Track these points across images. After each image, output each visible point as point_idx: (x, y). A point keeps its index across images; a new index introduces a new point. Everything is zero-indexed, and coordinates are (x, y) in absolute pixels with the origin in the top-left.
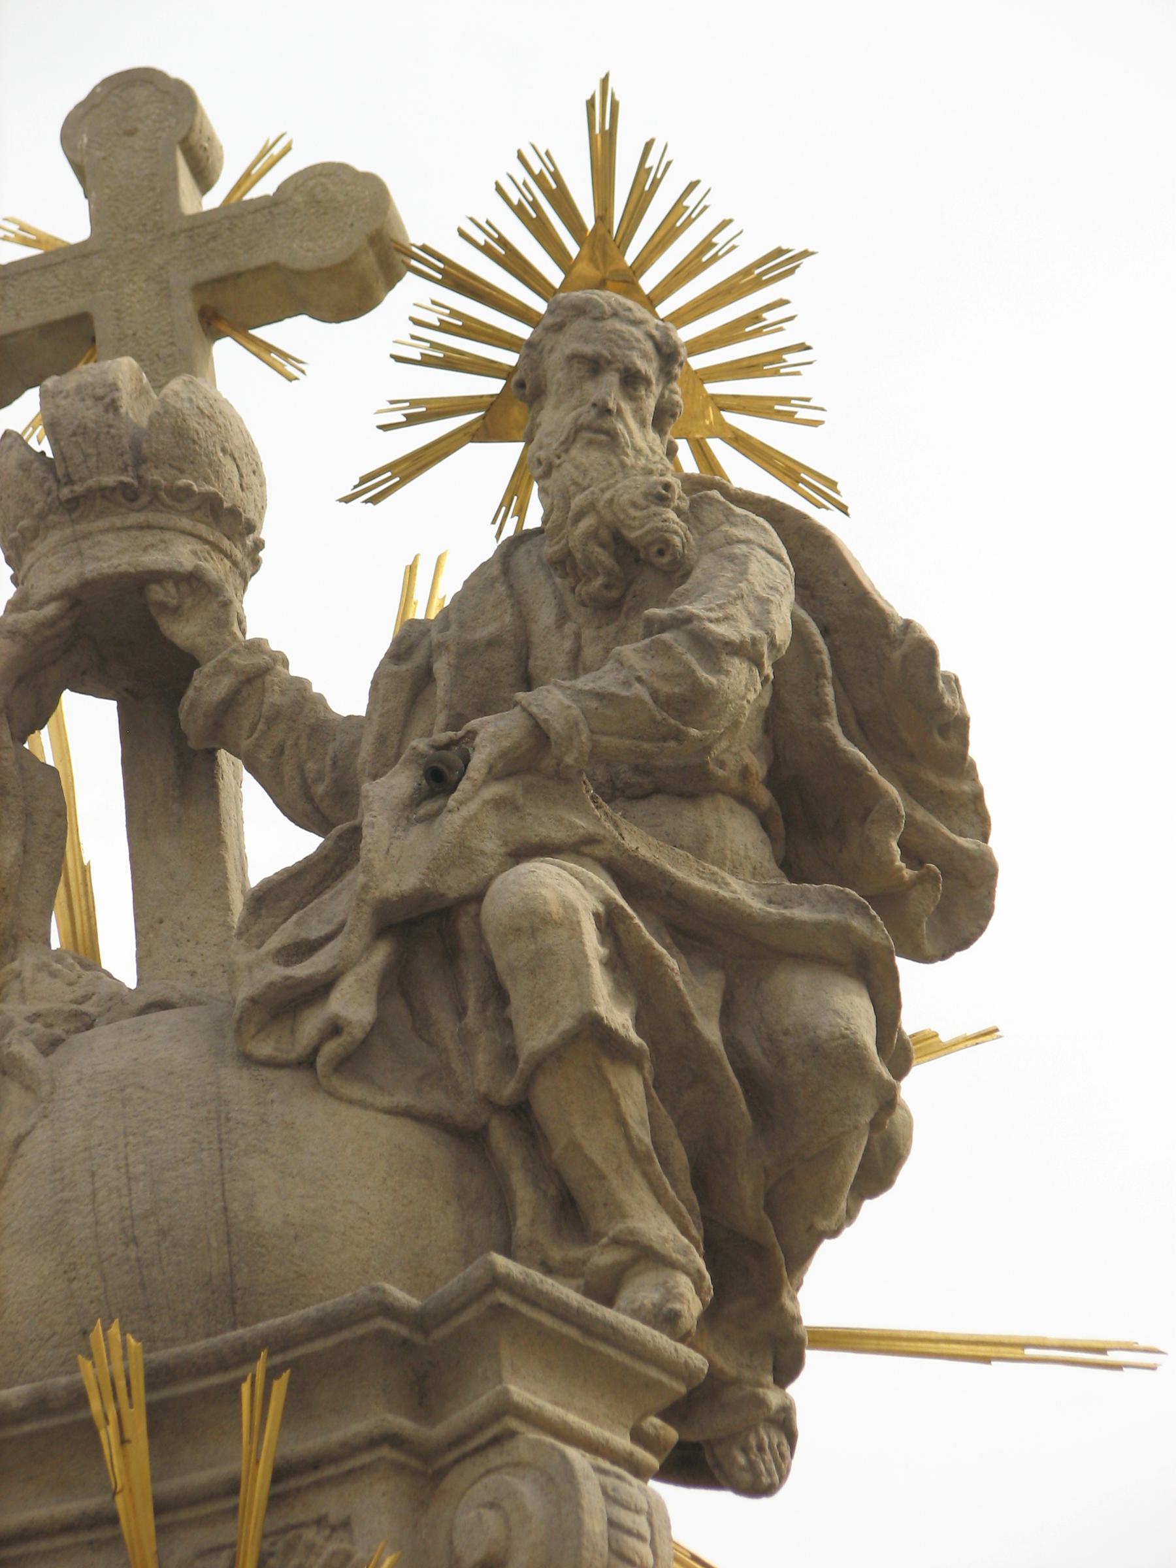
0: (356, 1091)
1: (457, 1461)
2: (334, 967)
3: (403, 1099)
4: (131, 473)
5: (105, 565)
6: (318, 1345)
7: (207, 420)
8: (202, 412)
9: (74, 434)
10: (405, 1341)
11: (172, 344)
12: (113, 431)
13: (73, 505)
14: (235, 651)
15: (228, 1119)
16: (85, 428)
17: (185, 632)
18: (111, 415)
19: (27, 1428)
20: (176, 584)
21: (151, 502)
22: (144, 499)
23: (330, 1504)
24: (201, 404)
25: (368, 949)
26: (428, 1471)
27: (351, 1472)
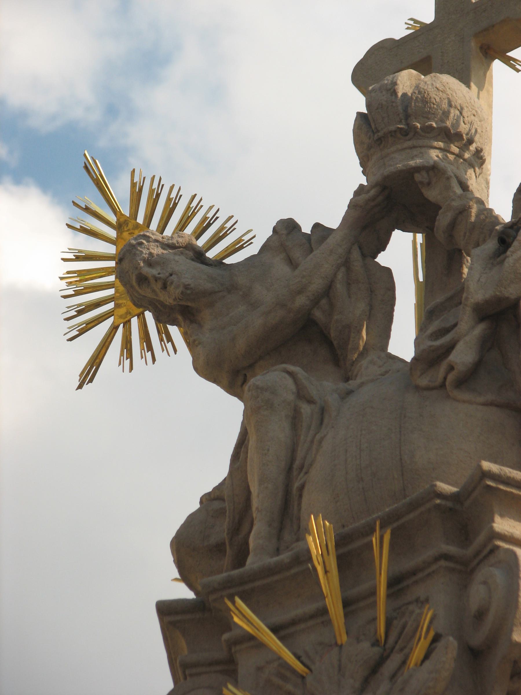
0: (466, 396)
1: (478, 564)
2: (453, 339)
3: (490, 397)
4: (404, 123)
5: (392, 168)
6: (411, 516)
7: (441, 93)
8: (438, 89)
9: (377, 109)
10: (451, 509)
11: (463, 63)
12: (394, 104)
13: (380, 141)
14: (453, 200)
15: (405, 417)
16: (382, 105)
17: (432, 194)
18: (394, 97)
19: (293, 571)
20: (428, 172)
21: (414, 135)
22: (411, 134)
23: (420, 591)
24: (438, 86)
25: (473, 328)
26: (464, 570)
27: (429, 575)
